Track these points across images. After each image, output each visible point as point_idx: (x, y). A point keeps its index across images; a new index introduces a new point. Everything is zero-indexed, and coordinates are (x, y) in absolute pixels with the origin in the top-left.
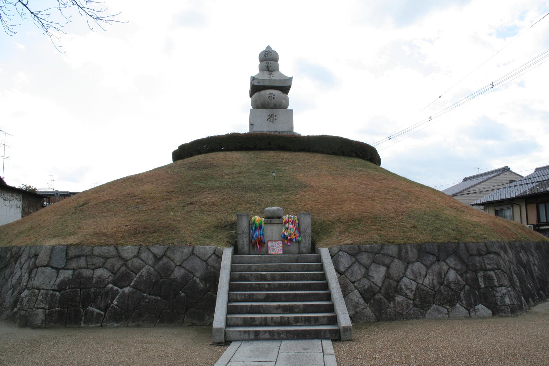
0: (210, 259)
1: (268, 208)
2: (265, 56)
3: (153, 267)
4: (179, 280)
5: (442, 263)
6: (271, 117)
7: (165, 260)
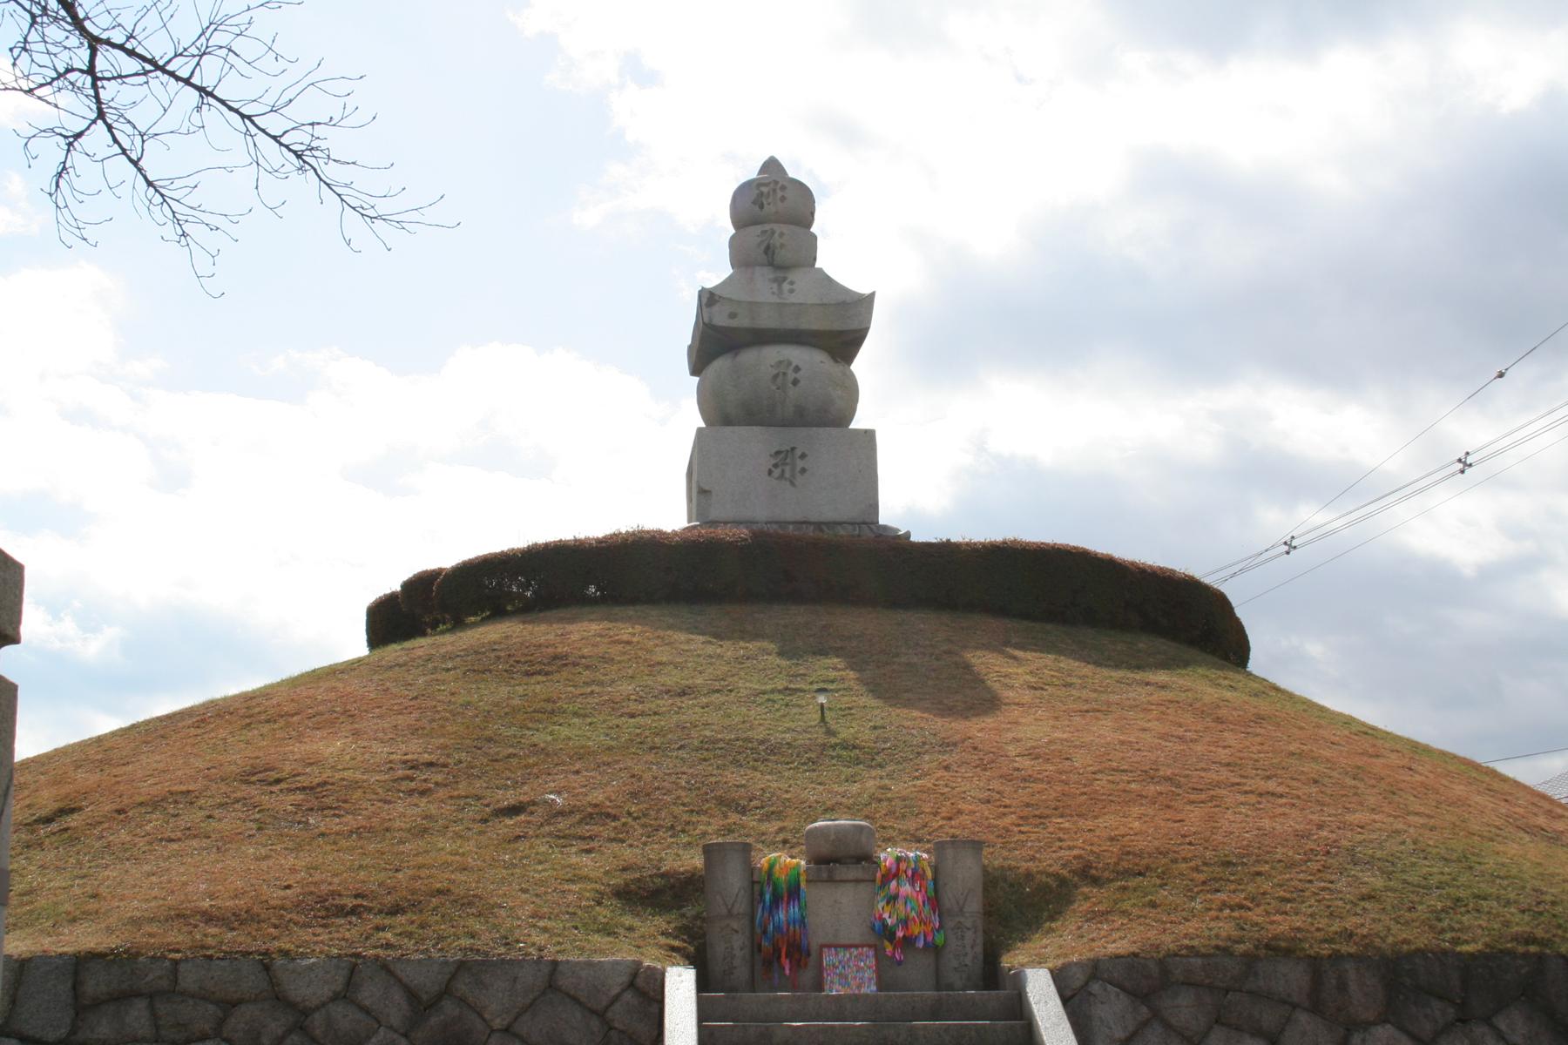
0: (617, 1007)
3: (405, 1035)
5: (1480, 1030)
6: (785, 463)
7: (449, 1008)
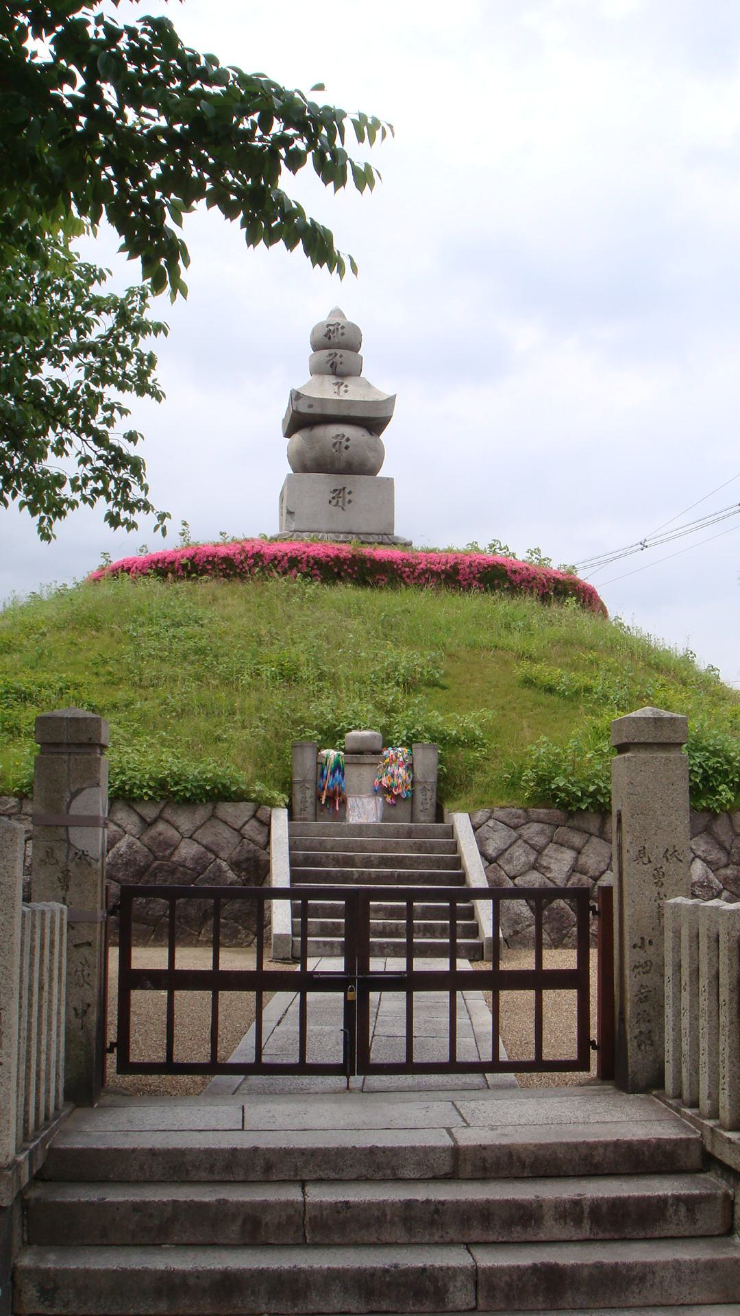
0: (247, 827)
1: (354, 733)
2: (328, 335)
4: (189, 864)
7: (161, 827)
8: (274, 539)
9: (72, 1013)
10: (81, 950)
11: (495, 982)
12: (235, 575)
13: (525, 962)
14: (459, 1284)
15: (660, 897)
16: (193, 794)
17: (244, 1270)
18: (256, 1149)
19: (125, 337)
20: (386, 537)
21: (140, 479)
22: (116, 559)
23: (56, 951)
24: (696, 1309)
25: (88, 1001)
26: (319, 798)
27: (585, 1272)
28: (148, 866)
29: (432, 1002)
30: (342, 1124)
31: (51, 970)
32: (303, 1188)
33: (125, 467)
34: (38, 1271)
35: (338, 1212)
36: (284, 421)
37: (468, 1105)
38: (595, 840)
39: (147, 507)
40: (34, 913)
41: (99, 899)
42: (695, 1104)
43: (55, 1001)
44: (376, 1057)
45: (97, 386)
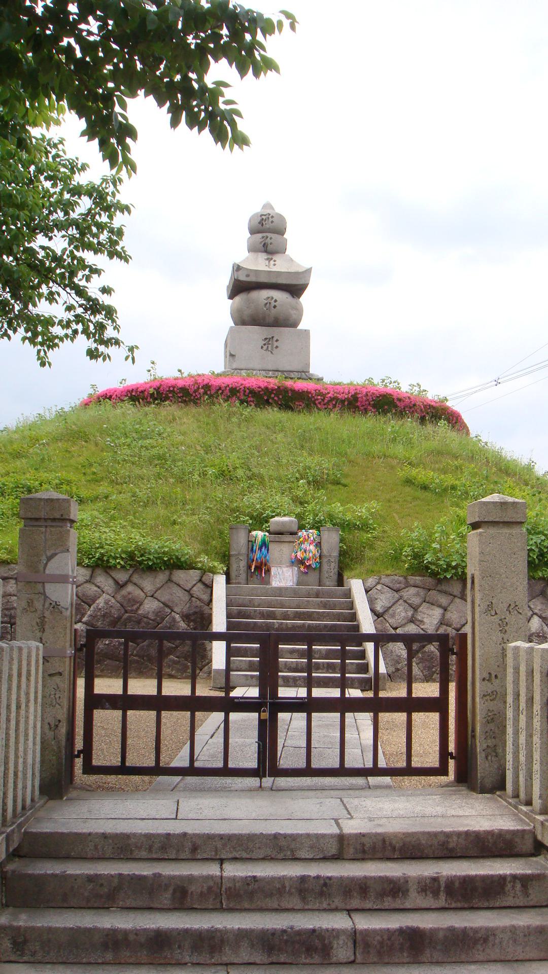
0: (195, 588)
1: (277, 519)
2: (261, 223)
4: (151, 616)
6: (269, 342)
7: (130, 588)
8: (219, 375)
9: (47, 727)
10: (54, 678)
11: (376, 706)
12: (190, 400)
13: (399, 692)
14: (341, 942)
15: (505, 641)
16: (154, 563)
17: (173, 930)
18: (185, 834)
19: (100, 215)
20: (304, 374)
21: (113, 321)
22: (102, 388)
23: (33, 678)
24: (527, 964)
25: (59, 717)
26: (249, 567)
27: (441, 935)
28: (120, 618)
29: (326, 722)
30: (254, 815)
31: (27, 694)
32: (221, 865)
33: (100, 313)
34: (11, 927)
35: (248, 884)
36: (228, 287)
37: (353, 802)
38: (457, 600)
39: (117, 342)
40: (12, 649)
41: (68, 638)
42: (529, 803)
43: (32, 718)
44: (284, 762)
45: (78, 251)
